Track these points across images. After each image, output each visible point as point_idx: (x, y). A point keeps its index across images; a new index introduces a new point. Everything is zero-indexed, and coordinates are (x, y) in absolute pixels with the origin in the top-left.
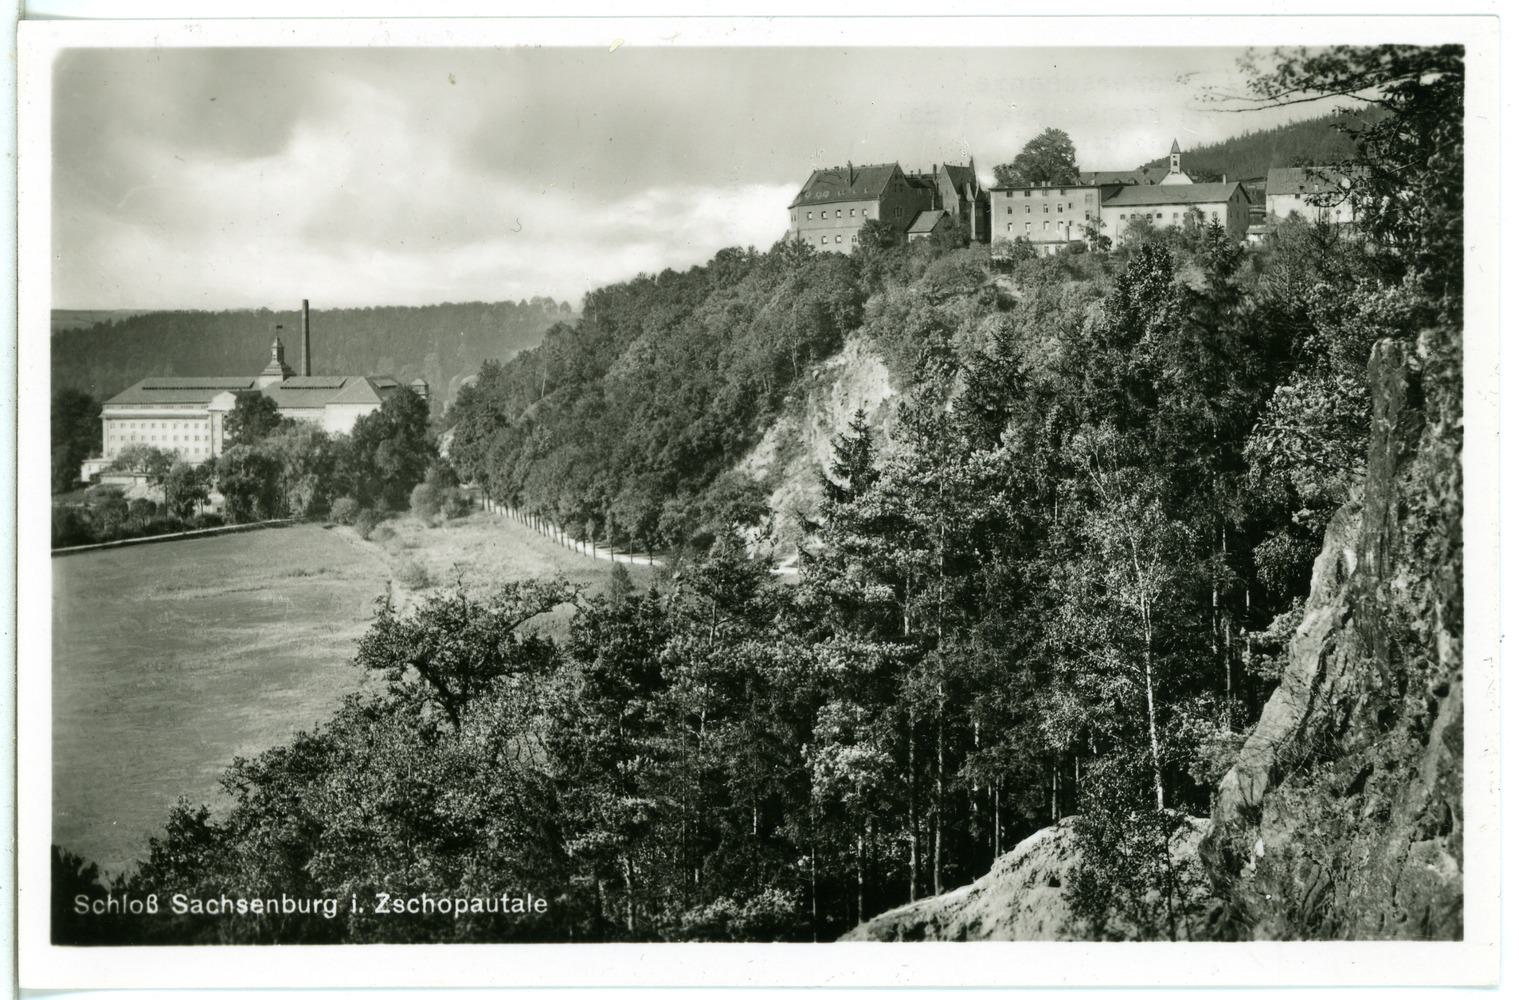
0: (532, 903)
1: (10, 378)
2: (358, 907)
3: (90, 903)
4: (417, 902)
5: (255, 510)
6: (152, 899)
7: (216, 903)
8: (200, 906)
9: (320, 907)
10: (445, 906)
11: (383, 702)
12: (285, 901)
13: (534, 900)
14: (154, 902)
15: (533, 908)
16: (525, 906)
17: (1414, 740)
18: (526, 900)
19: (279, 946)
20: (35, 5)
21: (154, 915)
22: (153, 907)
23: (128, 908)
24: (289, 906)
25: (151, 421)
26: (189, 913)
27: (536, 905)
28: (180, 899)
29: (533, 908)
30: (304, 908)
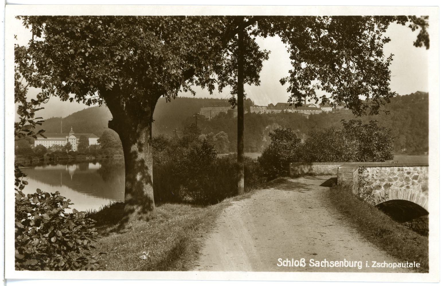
0: (415, 265)
1: (3, 184)
2: (368, 265)
5: (129, 207)
6: (303, 260)
8: (319, 264)
9: (357, 264)
10: (297, 263)
11: (87, 262)
13: (416, 264)
14: (304, 262)
15: (416, 266)
16: (413, 265)
17: (69, 257)
18: (413, 263)
19: (14, 242)
21: (279, 258)
22: (303, 263)
23: (415, 265)
25: (59, 141)
27: (417, 265)
29: (416, 266)
30: (351, 265)
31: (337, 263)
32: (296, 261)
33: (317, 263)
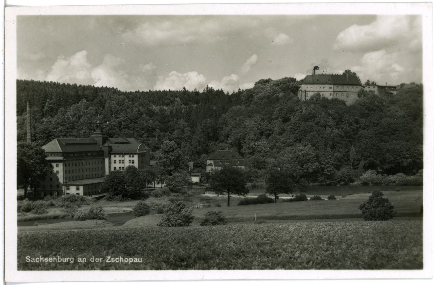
0: (129, 260)
3: (48, 259)
4: (39, 259)
7: (39, 259)
8: (34, 260)
12: (59, 259)
20: (8, 3)
24: (60, 260)
26: (30, 262)
28: (28, 258)
30: (140, 260)
31: (50, 259)
32: (127, 262)
33: (97, 261)
